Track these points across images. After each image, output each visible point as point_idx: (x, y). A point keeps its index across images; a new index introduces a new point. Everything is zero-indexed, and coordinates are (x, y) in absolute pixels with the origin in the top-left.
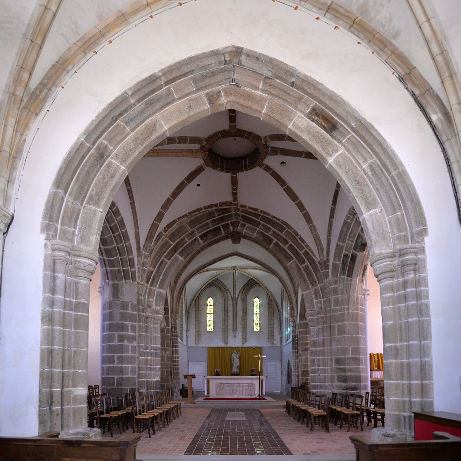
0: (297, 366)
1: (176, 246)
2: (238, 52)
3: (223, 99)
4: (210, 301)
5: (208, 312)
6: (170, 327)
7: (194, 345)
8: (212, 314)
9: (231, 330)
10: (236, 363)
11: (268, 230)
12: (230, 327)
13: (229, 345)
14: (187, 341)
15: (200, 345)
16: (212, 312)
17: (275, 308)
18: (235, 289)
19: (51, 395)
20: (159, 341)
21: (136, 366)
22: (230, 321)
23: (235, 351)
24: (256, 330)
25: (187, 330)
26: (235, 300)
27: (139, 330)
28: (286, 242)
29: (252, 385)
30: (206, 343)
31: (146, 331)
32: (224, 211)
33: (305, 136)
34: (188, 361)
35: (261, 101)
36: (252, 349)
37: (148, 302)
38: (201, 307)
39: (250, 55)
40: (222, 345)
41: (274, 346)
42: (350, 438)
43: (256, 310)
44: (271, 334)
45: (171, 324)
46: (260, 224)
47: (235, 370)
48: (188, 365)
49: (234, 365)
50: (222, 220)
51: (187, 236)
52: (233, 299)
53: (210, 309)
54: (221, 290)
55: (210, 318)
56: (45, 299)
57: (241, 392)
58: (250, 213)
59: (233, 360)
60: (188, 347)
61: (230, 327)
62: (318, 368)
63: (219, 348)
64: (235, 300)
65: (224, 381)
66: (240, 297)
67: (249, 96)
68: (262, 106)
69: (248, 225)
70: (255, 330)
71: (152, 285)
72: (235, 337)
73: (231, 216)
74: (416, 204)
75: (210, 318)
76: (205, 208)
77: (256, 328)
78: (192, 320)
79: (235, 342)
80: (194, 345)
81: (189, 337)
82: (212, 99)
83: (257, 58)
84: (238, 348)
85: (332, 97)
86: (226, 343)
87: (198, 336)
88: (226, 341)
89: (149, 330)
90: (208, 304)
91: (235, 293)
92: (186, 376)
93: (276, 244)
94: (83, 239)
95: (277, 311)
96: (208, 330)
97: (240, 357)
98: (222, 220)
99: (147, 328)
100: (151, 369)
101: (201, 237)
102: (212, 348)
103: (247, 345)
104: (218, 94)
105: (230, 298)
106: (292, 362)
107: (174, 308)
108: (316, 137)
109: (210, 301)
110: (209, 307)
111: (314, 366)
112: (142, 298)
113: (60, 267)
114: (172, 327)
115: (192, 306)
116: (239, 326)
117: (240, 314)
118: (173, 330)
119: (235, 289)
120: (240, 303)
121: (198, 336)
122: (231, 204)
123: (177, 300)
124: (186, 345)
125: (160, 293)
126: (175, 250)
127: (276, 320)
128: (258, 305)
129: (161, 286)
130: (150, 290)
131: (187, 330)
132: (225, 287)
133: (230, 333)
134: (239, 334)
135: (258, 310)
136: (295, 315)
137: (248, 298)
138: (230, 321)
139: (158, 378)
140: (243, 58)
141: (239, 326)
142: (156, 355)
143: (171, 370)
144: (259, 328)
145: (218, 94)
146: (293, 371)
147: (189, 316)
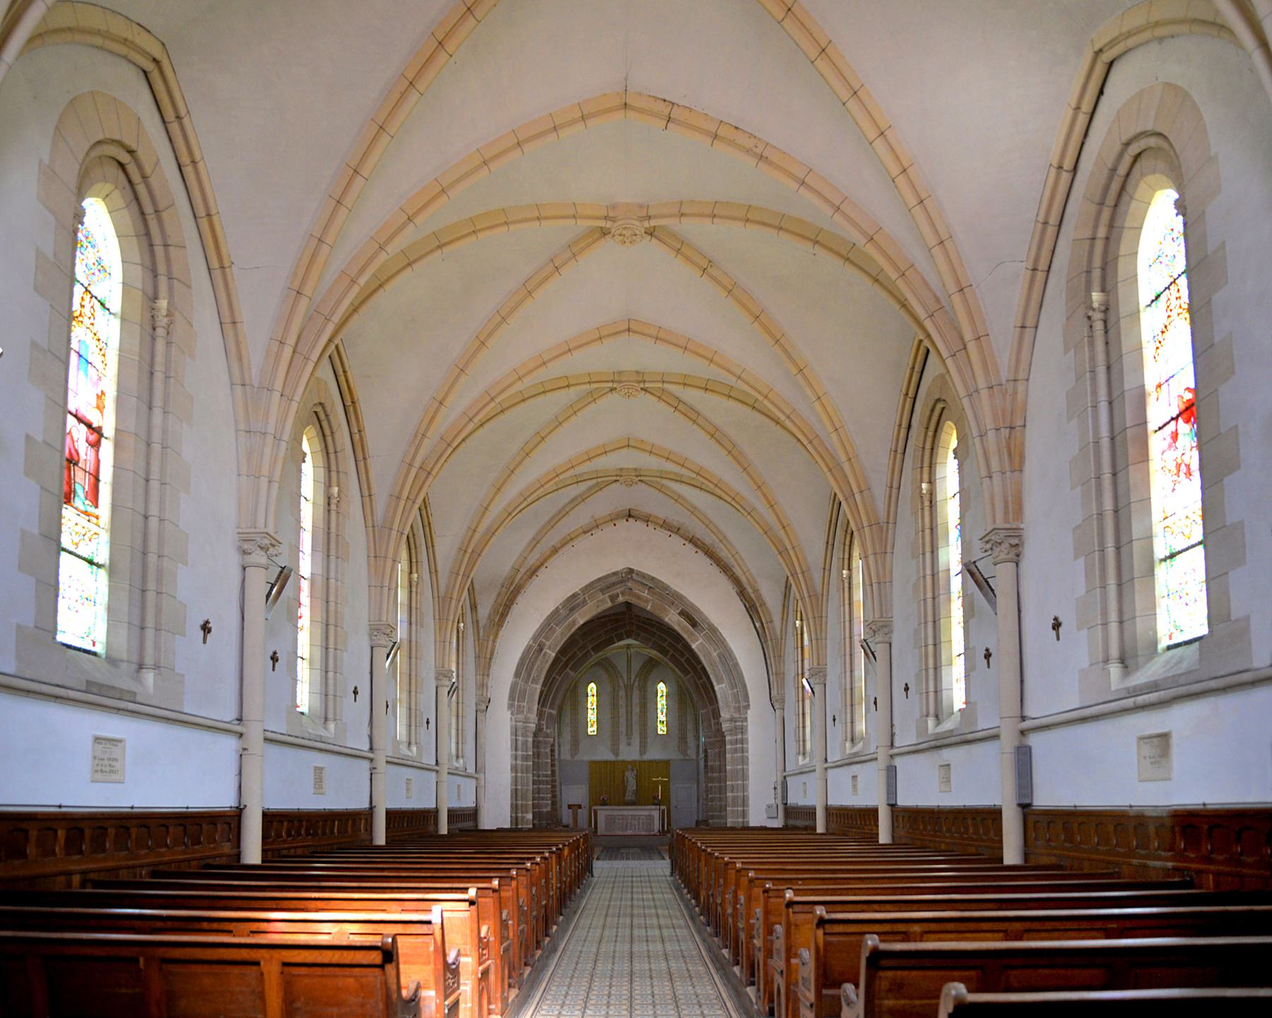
2: (631, 571)
4: (592, 688)
10: (632, 785)
12: (623, 729)
13: (620, 758)
15: (577, 758)
18: (629, 672)
19: (517, 818)
22: (623, 720)
24: (660, 732)
26: (629, 689)
28: (682, 655)
29: (651, 817)
30: (586, 756)
33: (676, 628)
35: (647, 601)
39: (639, 573)
40: (611, 757)
42: (97, 507)
43: (662, 703)
44: (683, 739)
47: (629, 797)
53: (592, 701)
55: (592, 716)
61: (623, 729)
63: (606, 762)
64: (629, 689)
65: (615, 813)
67: (639, 597)
68: (648, 602)
70: (660, 732)
72: (629, 744)
74: (745, 686)
75: (592, 716)
77: (662, 729)
79: (630, 753)
80: (568, 758)
82: (612, 598)
83: (644, 576)
84: (634, 762)
85: (693, 606)
86: (617, 755)
87: (575, 744)
88: (616, 751)
92: (570, 807)
94: (530, 710)
100: (543, 799)
102: (595, 762)
103: (648, 757)
108: (687, 632)
109: (592, 688)
110: (590, 699)
113: (519, 733)
116: (636, 728)
117: (636, 710)
119: (629, 672)
120: (636, 693)
127: (690, 718)
133: (623, 738)
134: (636, 740)
137: (649, 683)
138: (623, 720)
139: (549, 809)
141: (636, 728)
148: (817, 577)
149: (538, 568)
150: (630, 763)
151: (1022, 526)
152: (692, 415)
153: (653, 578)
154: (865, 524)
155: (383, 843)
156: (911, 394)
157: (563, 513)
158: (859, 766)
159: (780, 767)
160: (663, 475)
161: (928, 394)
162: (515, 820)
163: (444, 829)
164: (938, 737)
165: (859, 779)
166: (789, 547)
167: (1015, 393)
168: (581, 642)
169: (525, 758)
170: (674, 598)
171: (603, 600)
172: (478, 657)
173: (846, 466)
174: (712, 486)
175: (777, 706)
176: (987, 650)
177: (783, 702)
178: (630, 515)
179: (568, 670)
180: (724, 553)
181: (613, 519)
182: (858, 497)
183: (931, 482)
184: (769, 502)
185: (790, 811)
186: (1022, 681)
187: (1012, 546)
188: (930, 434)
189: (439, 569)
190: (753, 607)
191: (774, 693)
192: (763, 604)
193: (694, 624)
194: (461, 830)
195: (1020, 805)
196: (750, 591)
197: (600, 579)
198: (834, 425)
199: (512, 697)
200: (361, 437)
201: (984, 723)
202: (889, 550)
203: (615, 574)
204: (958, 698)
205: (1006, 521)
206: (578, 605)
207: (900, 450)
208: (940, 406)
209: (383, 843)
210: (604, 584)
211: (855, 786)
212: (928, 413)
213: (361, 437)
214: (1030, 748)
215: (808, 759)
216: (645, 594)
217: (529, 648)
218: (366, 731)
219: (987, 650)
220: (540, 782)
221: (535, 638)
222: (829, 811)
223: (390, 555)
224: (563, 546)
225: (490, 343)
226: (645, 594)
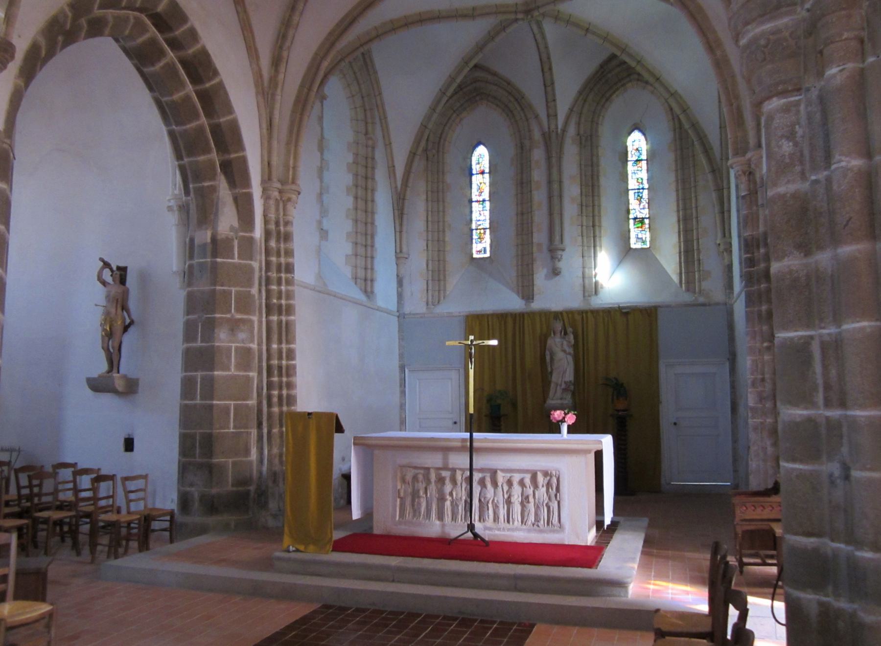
0: (768, 386)
4: (481, 157)
6: (258, 233)
7: (421, 308)
8: (487, 204)
9: (545, 248)
13: (537, 305)
15: (443, 309)
16: (486, 195)
17: (702, 159)
18: (550, 100)
23: (558, 326)
24: (639, 246)
26: (552, 143)
30: (461, 301)
34: (402, 368)
36: (589, 314)
38: (449, 179)
40: (513, 303)
41: (701, 300)
43: (637, 175)
45: (266, 221)
49: (555, 378)
52: (547, 137)
54: (508, 111)
55: (481, 215)
57: (502, 512)
59: (552, 359)
60: (401, 316)
62: (835, 413)
66: (572, 130)
70: (634, 244)
75: (481, 215)
80: (421, 308)
81: (406, 282)
90: (475, 168)
91: (552, 115)
95: (707, 168)
96: (475, 256)
97: (575, 346)
105: (537, 135)
106: (749, 363)
107: (275, 160)
109: (481, 157)
110: (476, 180)
111: (805, 399)
114: (267, 234)
115: (412, 175)
118: (273, 244)
121: (437, 275)
123: (291, 131)
124: (393, 306)
128: (644, 157)
132: (518, 98)
135: (644, 175)
136: (752, 141)
137: (605, 131)
143: (260, 403)
144: (647, 236)
146: (753, 409)
147: (406, 211)
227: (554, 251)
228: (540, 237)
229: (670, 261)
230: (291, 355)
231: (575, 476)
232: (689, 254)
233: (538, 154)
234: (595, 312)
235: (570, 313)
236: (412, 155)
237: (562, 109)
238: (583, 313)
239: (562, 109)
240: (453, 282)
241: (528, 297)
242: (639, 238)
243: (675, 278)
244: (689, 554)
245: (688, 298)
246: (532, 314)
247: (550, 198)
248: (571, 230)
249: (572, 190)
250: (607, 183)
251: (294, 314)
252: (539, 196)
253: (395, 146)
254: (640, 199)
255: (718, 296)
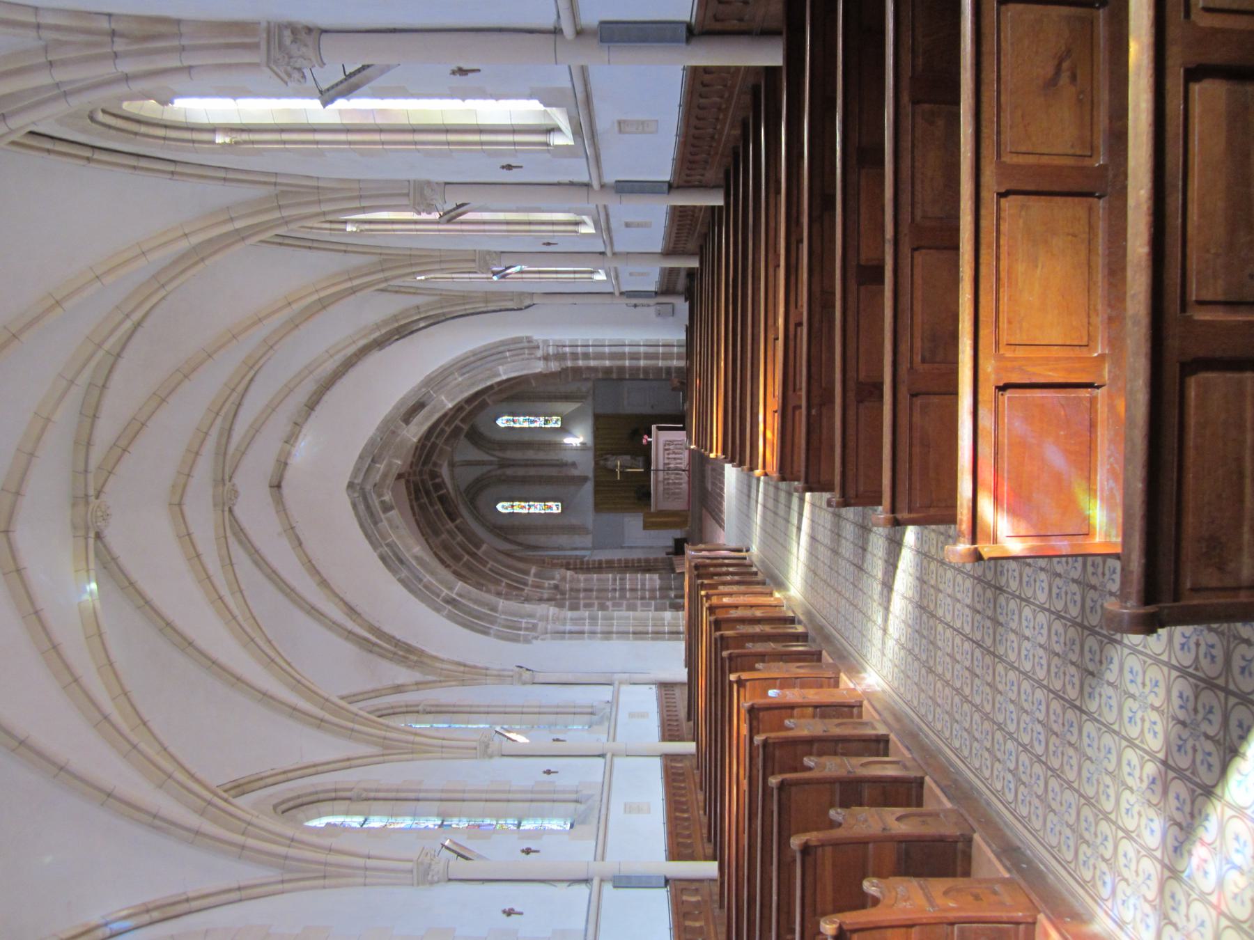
1: (468, 553)
2: (351, 485)
3: (387, 497)
4: (503, 507)
5: (525, 511)
7: (590, 538)
11: (443, 431)
13: (590, 474)
14: (583, 549)
16: (526, 504)
20: (603, 576)
21: (639, 602)
23: (602, 462)
24: (559, 425)
25: (560, 548)
26: (504, 464)
27: (590, 598)
30: (588, 517)
31: (591, 590)
32: (417, 491)
35: (390, 465)
37: (549, 588)
40: (589, 487)
43: (522, 422)
46: (434, 443)
48: (631, 547)
50: (428, 493)
51: (454, 539)
53: (519, 508)
55: (537, 508)
56: (590, 638)
58: (420, 456)
66: (497, 453)
67: (385, 476)
69: (434, 458)
70: (559, 425)
71: (526, 584)
73: (423, 481)
75: (537, 508)
76: (414, 514)
78: (542, 540)
80: (590, 538)
82: (386, 508)
83: (357, 470)
85: (396, 408)
89: (589, 587)
90: (510, 510)
91: (491, 463)
93: (463, 420)
98: (428, 493)
99: (585, 590)
100: (643, 584)
101: (453, 520)
104: (383, 502)
105: (499, 472)
108: (427, 418)
109: (503, 507)
110: (517, 510)
112: (546, 596)
113: (561, 628)
121: (572, 530)
122: (408, 482)
125: (536, 575)
126: (473, 555)
129: (527, 573)
130: (533, 586)
131: (560, 548)
132: (478, 481)
135: (521, 419)
137: (498, 437)
139: (656, 576)
140: (356, 481)
142: (622, 579)
144: (555, 418)
145: (383, 502)
148: (355, 261)
149: (346, 604)
150: (596, 463)
151: (264, 25)
152: (134, 429)
153: (361, 457)
154: (277, 215)
155: (716, 864)
156: (88, 153)
157: (274, 576)
158: (612, 220)
159: (608, 299)
160: (221, 452)
161: (83, 131)
162: (674, 634)
163: (690, 747)
164: (577, 132)
165: (629, 220)
166: (316, 297)
167: (57, 28)
168: (444, 536)
169: (593, 619)
170: (388, 431)
171: (389, 520)
172: (463, 682)
173: (195, 240)
174: (235, 394)
175: (527, 302)
176: (454, 73)
177: (522, 294)
178: (278, 486)
179: (480, 553)
180: (330, 366)
181: (279, 502)
182: (238, 224)
183: (214, 129)
184: (254, 324)
185: (667, 289)
186: (500, 30)
187: (294, 41)
188: (143, 129)
189: (343, 755)
190: (401, 331)
191: (510, 305)
192: (395, 318)
193: (420, 406)
194: (689, 719)
195: (688, 40)
196: (377, 334)
197: (362, 526)
198: (136, 257)
199: (515, 639)
200: (157, 908)
201: (561, 78)
202: (314, 183)
203: (354, 506)
204: (524, 110)
205: (256, 46)
206: (396, 554)
207: (171, 168)
208: (101, 117)
209: (716, 864)
210: (368, 517)
211: (639, 225)
212: (112, 132)
213: (157, 908)
214: (602, 23)
215: (585, 218)
216: (381, 467)
217: (451, 617)
218: (562, 889)
219: (454, 73)
220: (623, 589)
221: (438, 609)
222: (671, 251)
223: (321, 856)
224: (318, 572)
225: (149, 424)
226: (381, 467)
227: (563, 465)
228: (554, 472)
229: (569, 407)
230: (619, 561)
231: (665, 436)
232: (567, 398)
233: (509, 472)
234: (596, 444)
235: (595, 456)
236: (506, 539)
237: (486, 458)
238: (596, 450)
239: (486, 458)
240: (574, 521)
241: (585, 479)
242: (555, 423)
243: (578, 405)
244: (539, 367)
245: (590, 398)
246: (595, 477)
247: (534, 465)
248: (552, 456)
249: (530, 455)
250: (526, 438)
251: (663, 270)
252: (532, 472)
253: (309, 759)
254: (534, 421)
255: (590, 384)
